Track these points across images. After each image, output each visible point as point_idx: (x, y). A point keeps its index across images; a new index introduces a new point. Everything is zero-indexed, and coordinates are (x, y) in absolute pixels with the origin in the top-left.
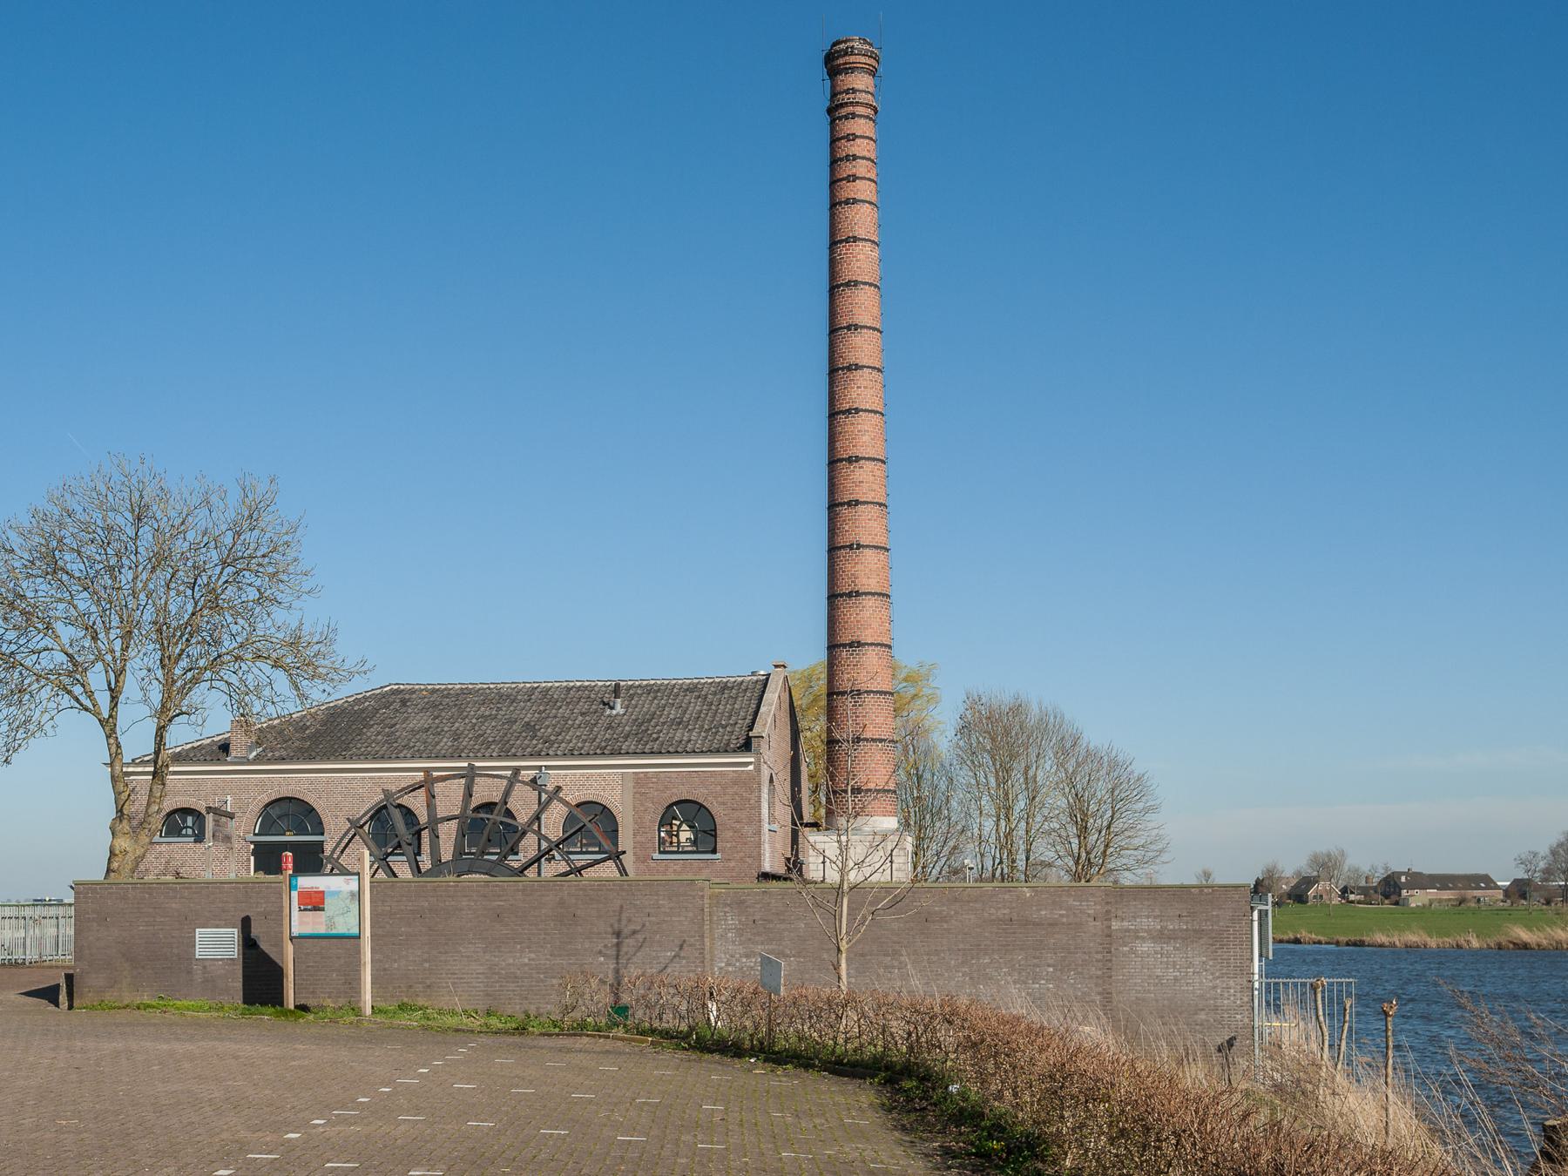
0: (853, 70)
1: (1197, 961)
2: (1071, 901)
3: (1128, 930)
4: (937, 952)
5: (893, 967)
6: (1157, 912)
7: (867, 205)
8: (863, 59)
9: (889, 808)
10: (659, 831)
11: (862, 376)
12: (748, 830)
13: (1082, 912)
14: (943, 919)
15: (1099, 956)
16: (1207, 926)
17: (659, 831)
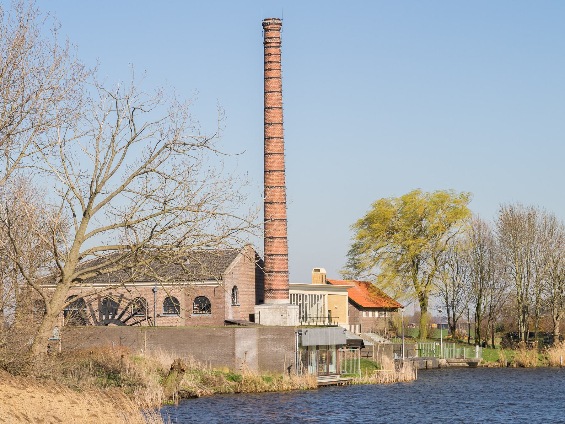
0: (270, 30)
1: (282, 346)
2: (225, 331)
3: (265, 338)
4: (193, 343)
5: (183, 346)
6: (272, 334)
7: (276, 79)
8: (274, 26)
9: (284, 296)
10: (193, 306)
11: (274, 141)
12: (221, 306)
13: (228, 333)
14: (195, 335)
15: (231, 344)
16: (284, 337)
17: (193, 306)
